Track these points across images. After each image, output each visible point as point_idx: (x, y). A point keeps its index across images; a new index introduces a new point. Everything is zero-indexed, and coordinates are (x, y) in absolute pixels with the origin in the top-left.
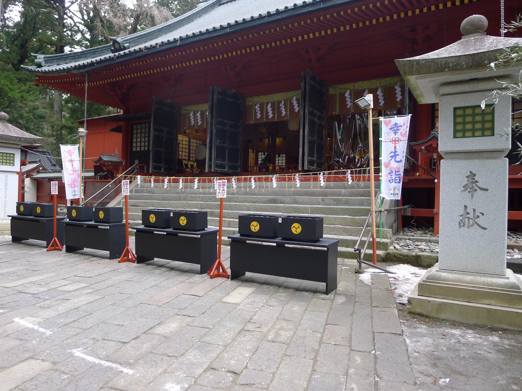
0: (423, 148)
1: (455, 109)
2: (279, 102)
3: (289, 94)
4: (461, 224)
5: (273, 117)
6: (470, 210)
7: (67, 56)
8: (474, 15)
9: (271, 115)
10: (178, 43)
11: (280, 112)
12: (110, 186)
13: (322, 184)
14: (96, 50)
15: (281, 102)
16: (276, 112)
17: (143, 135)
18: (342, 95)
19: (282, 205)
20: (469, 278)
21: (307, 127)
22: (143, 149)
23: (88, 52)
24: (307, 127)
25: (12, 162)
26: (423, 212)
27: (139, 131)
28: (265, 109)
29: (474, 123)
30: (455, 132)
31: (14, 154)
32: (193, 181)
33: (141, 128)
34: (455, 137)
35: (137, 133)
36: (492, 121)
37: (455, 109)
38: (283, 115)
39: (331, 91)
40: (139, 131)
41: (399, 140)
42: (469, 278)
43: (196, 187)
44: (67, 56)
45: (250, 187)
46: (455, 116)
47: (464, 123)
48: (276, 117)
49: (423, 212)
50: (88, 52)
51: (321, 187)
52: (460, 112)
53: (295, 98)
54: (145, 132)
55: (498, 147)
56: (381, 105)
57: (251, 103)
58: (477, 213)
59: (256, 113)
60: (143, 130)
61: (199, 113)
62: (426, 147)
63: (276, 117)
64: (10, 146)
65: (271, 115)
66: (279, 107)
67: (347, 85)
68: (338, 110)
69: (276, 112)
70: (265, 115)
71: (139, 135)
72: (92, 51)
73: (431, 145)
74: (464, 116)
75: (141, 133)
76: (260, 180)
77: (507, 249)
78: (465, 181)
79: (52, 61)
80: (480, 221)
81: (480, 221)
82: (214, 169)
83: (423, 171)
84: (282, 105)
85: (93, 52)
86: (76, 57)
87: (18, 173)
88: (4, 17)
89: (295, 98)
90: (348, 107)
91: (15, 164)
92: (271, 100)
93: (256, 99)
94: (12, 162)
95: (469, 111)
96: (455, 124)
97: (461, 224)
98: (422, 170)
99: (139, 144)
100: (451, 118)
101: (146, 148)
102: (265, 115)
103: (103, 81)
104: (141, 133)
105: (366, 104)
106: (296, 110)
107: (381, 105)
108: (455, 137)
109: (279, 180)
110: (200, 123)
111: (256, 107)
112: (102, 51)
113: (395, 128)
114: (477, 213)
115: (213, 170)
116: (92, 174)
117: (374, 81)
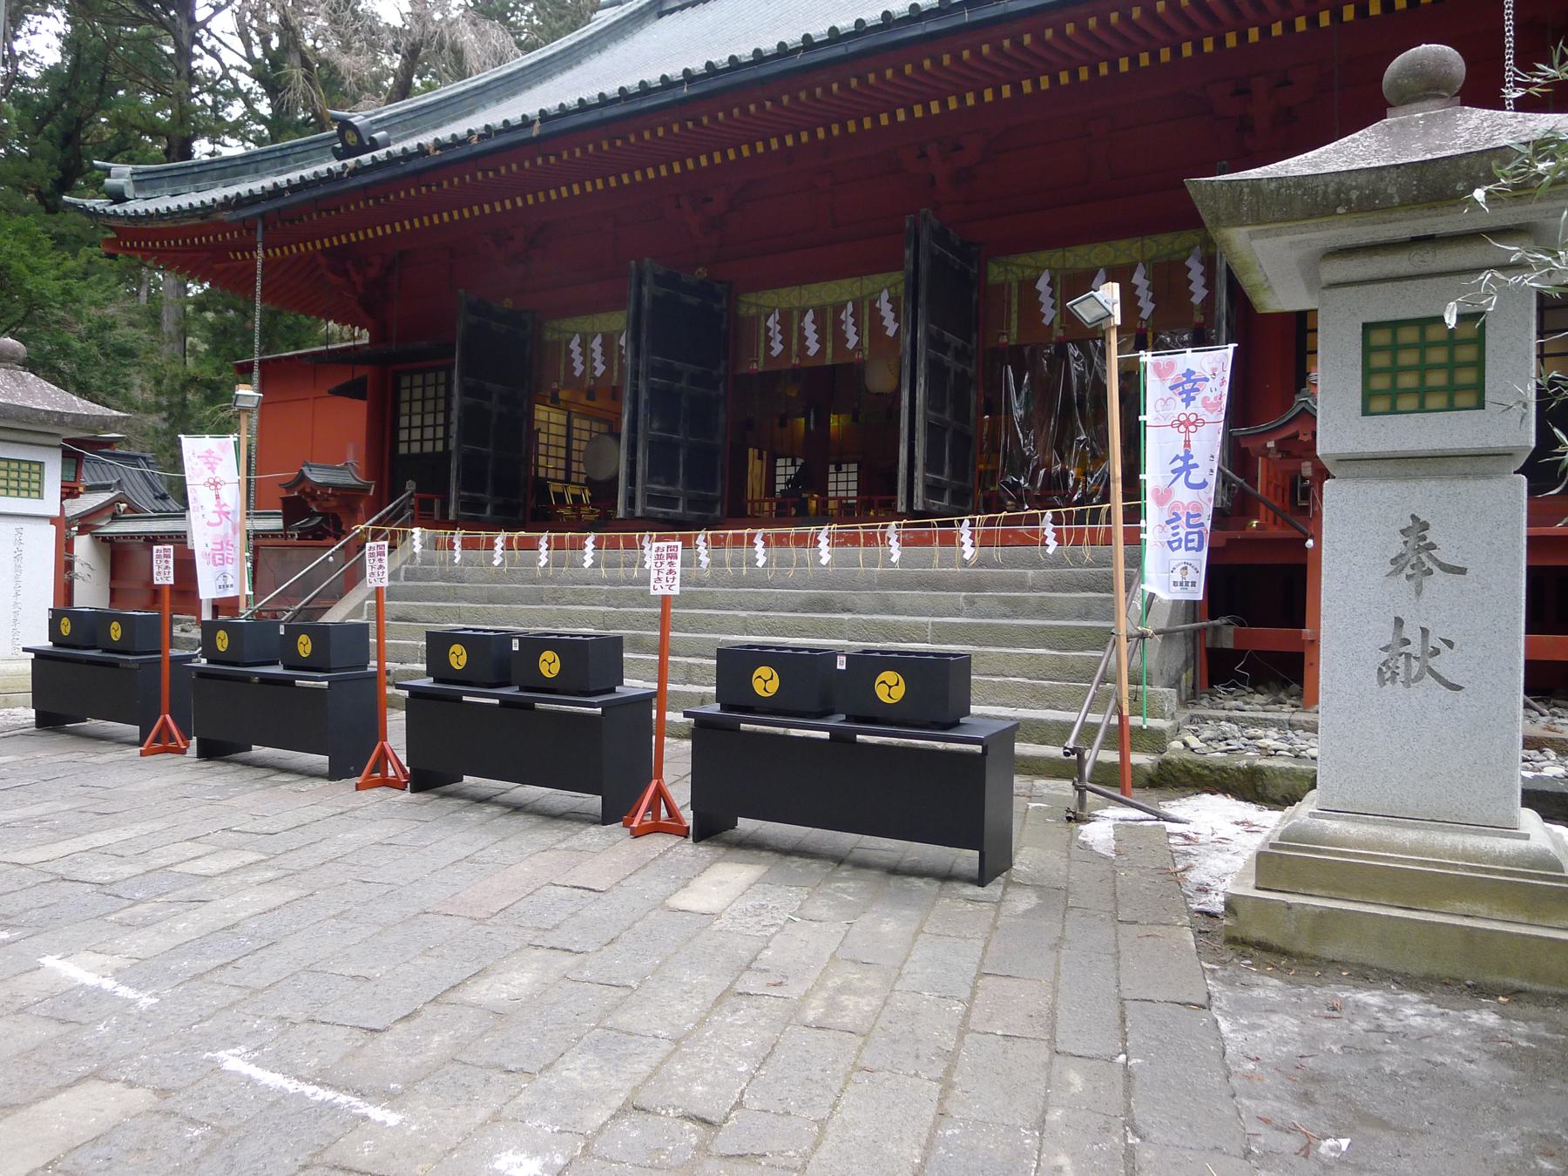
0: (1271, 444)
1: (1367, 327)
2: (839, 308)
3: (869, 283)
4: (1386, 674)
5: (821, 352)
6: (1411, 632)
7: (202, 168)
8: (1424, 45)
9: (813, 347)
10: (536, 131)
11: (840, 338)
12: (331, 559)
13: (969, 552)
14: (289, 151)
15: (844, 306)
16: (829, 336)
17: (430, 406)
18: (1029, 287)
19: (846, 616)
20: (1408, 836)
21: (921, 381)
22: (428, 447)
23: (266, 157)
24: (921, 381)
25: (35, 486)
26: (1271, 638)
27: (418, 393)
28: (795, 327)
29: (1423, 369)
30: (1368, 396)
31: (41, 464)
32: (579, 546)
33: (424, 386)
34: (1366, 411)
35: (411, 401)
36: (1479, 364)
37: (1367, 327)
38: (850, 345)
39: (995, 273)
40: (418, 393)
41: (1197, 422)
42: (1408, 836)
43: (588, 562)
44: (202, 168)
45: (752, 562)
46: (1368, 350)
47: (1395, 370)
48: (829, 351)
49: (1271, 638)
50: (266, 157)
51: (965, 563)
52: (1381, 338)
53: (885, 296)
54: (436, 398)
55: (1495, 442)
56: (1145, 315)
57: (753, 311)
58: (1434, 641)
59: (769, 339)
60: (430, 392)
61: (598, 340)
62: (1278, 443)
63: (829, 351)
64: (31, 438)
65: (813, 347)
66: (838, 323)
67: (1043, 256)
68: (1014, 330)
69: (829, 336)
70: (795, 347)
71: (417, 407)
72: (278, 154)
73: (1296, 436)
74: (1395, 348)
75: (423, 400)
76: (781, 540)
77: (1524, 748)
78: (1397, 546)
79: (156, 183)
80: (1441, 664)
81: (1441, 664)
82: (643, 510)
83: (1271, 514)
84: (847, 315)
85: (279, 157)
86: (229, 170)
87: (53, 520)
88: (11, 50)
89: (885, 296)
90: (1046, 321)
91: (46, 492)
92: (815, 302)
93: (768, 298)
94: (35, 486)
95: (1409, 335)
96: (1368, 372)
97: (1386, 674)
98: (1266, 512)
99: (416, 434)
100: (1356, 355)
101: (440, 446)
102: (795, 347)
103: (309, 244)
104: (423, 400)
105: (1100, 312)
106: (891, 332)
107: (1145, 315)
108: (1366, 411)
109: (837, 541)
110: (600, 369)
111: (770, 323)
112: (305, 154)
113: (1188, 386)
114: (1434, 641)
115: (638, 512)
116: (276, 524)
117: (1123, 244)
